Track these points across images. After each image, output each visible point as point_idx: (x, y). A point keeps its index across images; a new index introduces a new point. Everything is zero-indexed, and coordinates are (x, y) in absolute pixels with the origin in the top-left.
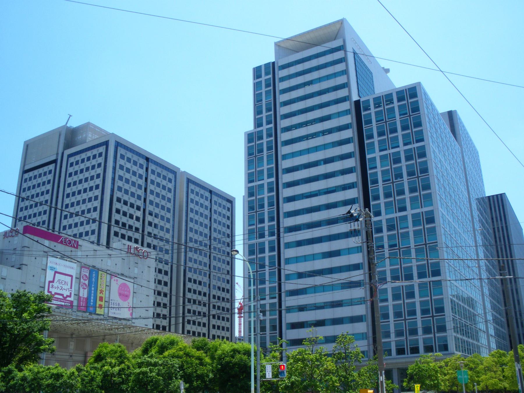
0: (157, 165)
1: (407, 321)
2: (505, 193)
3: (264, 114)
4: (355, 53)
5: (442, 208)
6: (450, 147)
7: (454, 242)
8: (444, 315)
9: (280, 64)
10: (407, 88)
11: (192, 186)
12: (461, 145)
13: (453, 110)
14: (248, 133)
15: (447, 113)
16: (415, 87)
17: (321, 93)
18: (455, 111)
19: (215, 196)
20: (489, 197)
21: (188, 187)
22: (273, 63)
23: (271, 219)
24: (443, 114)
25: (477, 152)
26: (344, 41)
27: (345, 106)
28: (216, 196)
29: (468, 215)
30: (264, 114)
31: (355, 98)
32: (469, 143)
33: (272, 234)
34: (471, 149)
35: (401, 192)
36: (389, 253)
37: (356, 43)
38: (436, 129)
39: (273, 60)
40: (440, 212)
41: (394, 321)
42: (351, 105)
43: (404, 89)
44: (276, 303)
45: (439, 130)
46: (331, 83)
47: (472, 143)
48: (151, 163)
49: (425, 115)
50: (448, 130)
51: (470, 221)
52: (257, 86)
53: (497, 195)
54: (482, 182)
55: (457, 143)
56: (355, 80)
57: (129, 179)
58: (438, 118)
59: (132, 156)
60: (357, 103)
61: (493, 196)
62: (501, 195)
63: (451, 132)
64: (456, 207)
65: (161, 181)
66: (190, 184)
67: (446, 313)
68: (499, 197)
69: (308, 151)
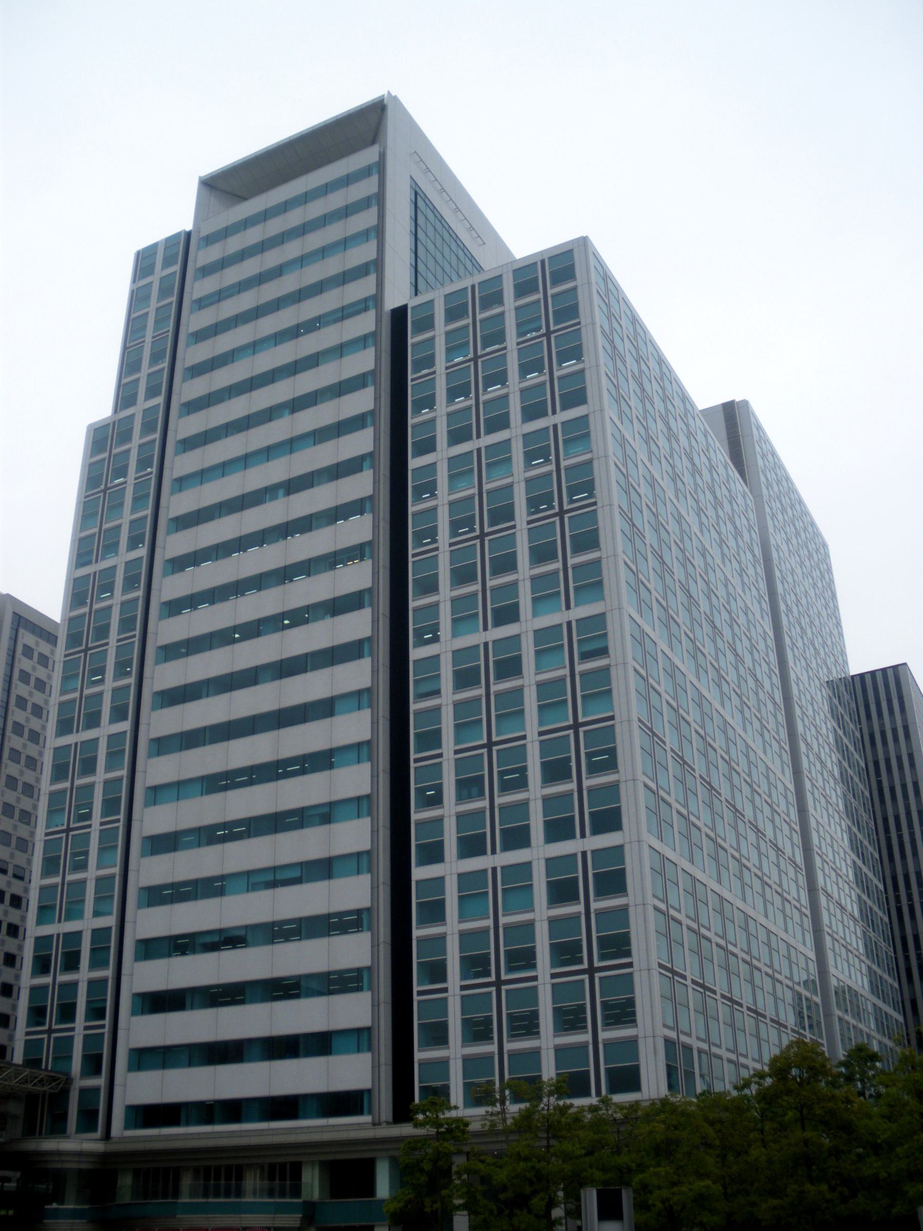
0: (40, 637)
1: (504, 988)
2: (905, 664)
3: (146, 369)
4: (417, 194)
5: (815, 809)
6: (833, 667)
7: (832, 872)
8: (630, 965)
9: (204, 233)
10: (546, 257)
11: (27, 638)
12: (758, 497)
13: (738, 399)
14: (97, 427)
15: (721, 408)
16: (570, 252)
17: (300, 296)
18: (745, 404)
19: (25, 632)
20: (862, 676)
21: (15, 639)
22: (188, 235)
23: (122, 669)
24: (708, 413)
25: (825, 545)
26: (383, 156)
27: (365, 324)
28: (33, 632)
29: (829, 764)
30: (146, 369)
31: (392, 301)
32: (817, 551)
33: (119, 714)
34: (812, 547)
35: (507, 564)
36: (456, 760)
37: (443, 190)
38: (802, 628)
39: (189, 227)
40: (626, 620)
41: (463, 988)
42: (378, 320)
43: (539, 259)
44: (110, 928)
45: (795, 609)
46: (332, 266)
47: (805, 513)
48: (25, 628)
49: (594, 331)
50: (721, 455)
51: (835, 779)
52: (137, 298)
53: (884, 670)
54: (838, 624)
55: (737, 475)
56: (408, 257)
57: (27, 697)
58: (794, 581)
59: (37, 644)
60: (399, 315)
61: (873, 673)
62: (895, 668)
63: (732, 459)
64: (822, 775)
65: (34, 669)
66: (21, 631)
67: (635, 959)
68: (890, 674)
69: (245, 461)
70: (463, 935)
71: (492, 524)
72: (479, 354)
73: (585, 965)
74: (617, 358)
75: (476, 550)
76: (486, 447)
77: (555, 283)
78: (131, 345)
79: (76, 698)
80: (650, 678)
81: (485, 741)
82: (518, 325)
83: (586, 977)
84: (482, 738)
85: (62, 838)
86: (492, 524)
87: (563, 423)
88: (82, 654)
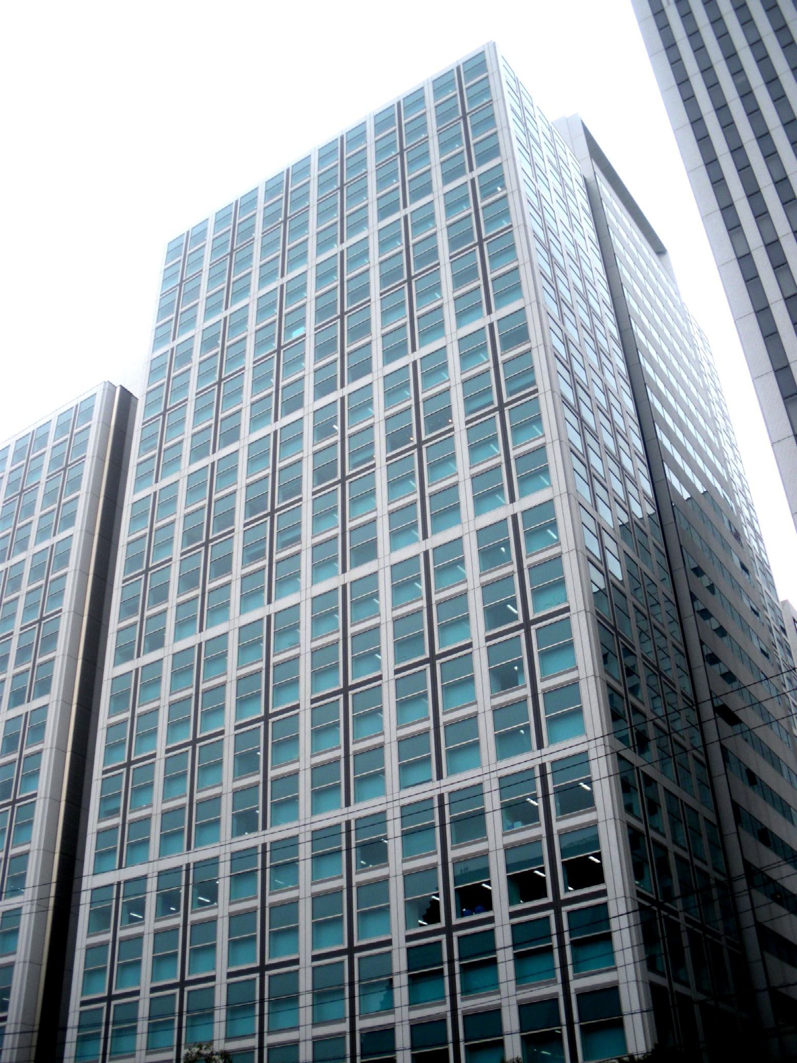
36: (409, 949)
70: (407, 875)
71: (430, 430)
72: (437, 652)
73: (550, 899)
74: (593, 316)
75: (425, 677)
76: (434, 549)
77: (506, 347)
78: (216, 535)
79: (185, 805)
80: (651, 617)
81: (427, 655)
82: (467, 401)
83: (551, 913)
84: (423, 653)
85: (174, 995)
86: (430, 430)
87: (523, 512)
88: (190, 748)
